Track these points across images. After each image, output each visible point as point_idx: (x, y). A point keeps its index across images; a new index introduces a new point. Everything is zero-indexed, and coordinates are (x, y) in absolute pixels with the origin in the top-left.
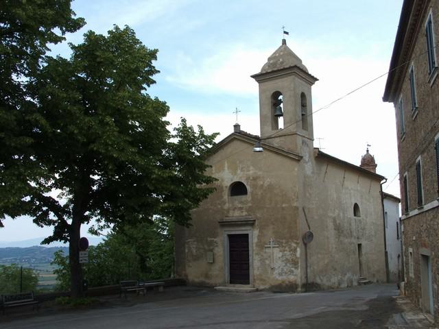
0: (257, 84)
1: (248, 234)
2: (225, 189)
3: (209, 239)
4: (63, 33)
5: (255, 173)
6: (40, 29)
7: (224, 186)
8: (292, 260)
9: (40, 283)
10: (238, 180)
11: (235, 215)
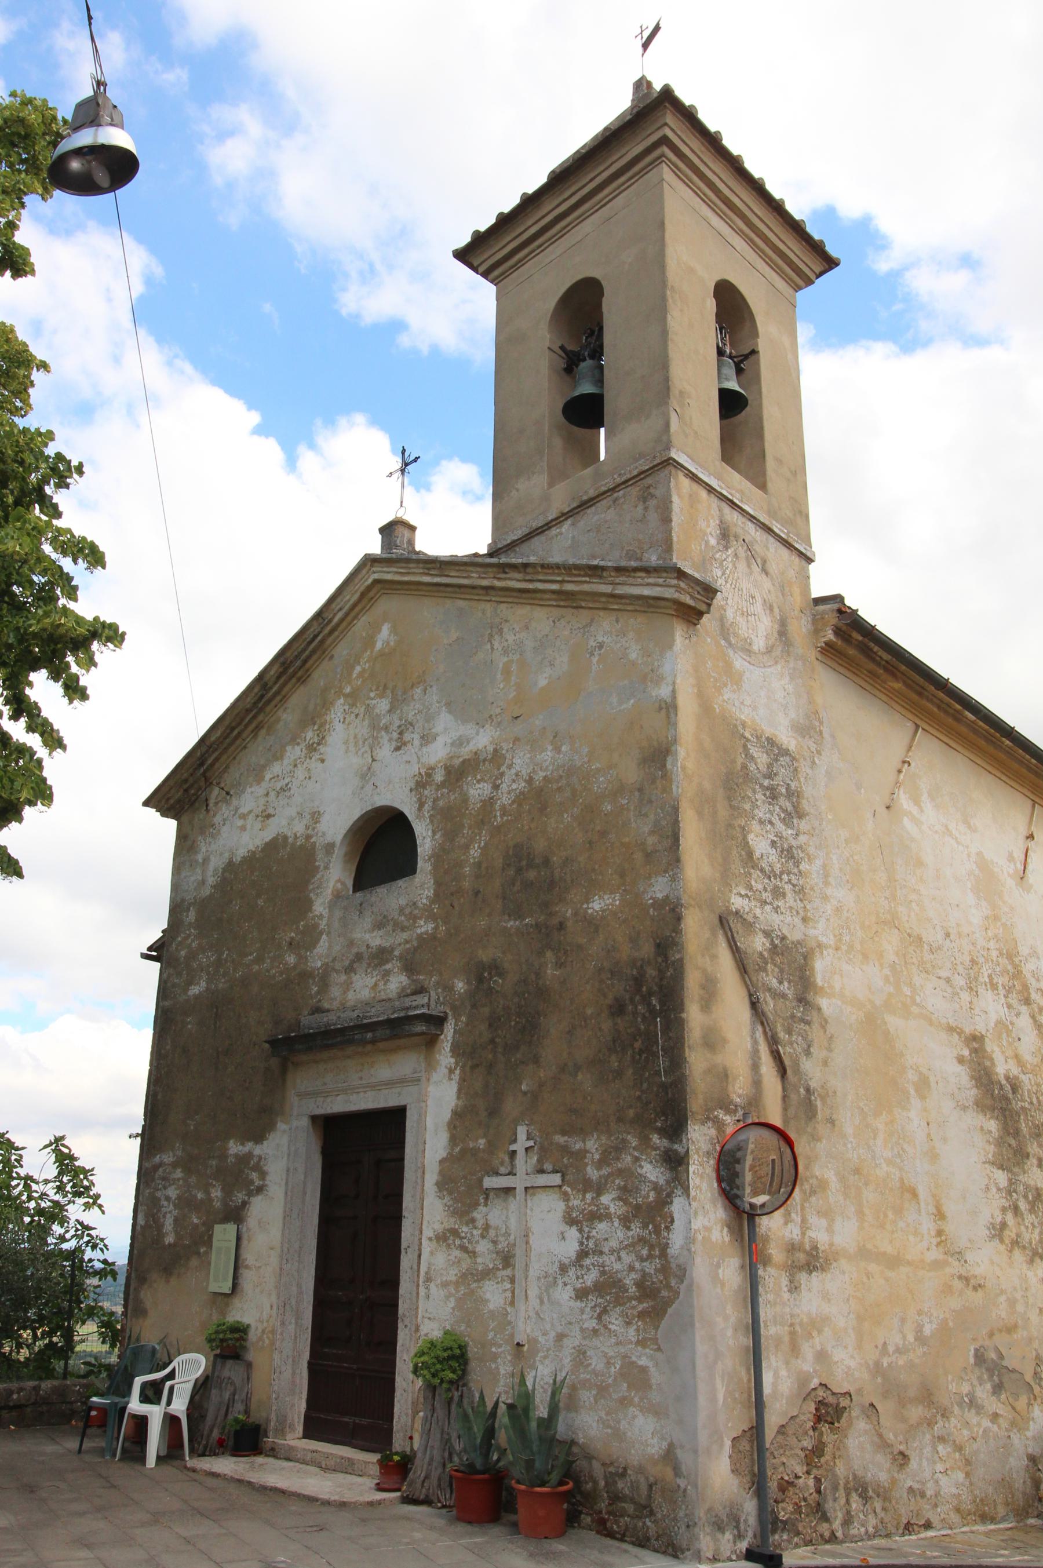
3: (234, 1148)
5: (460, 742)
7: (319, 841)
9: (1028, 1491)
10: (356, 814)
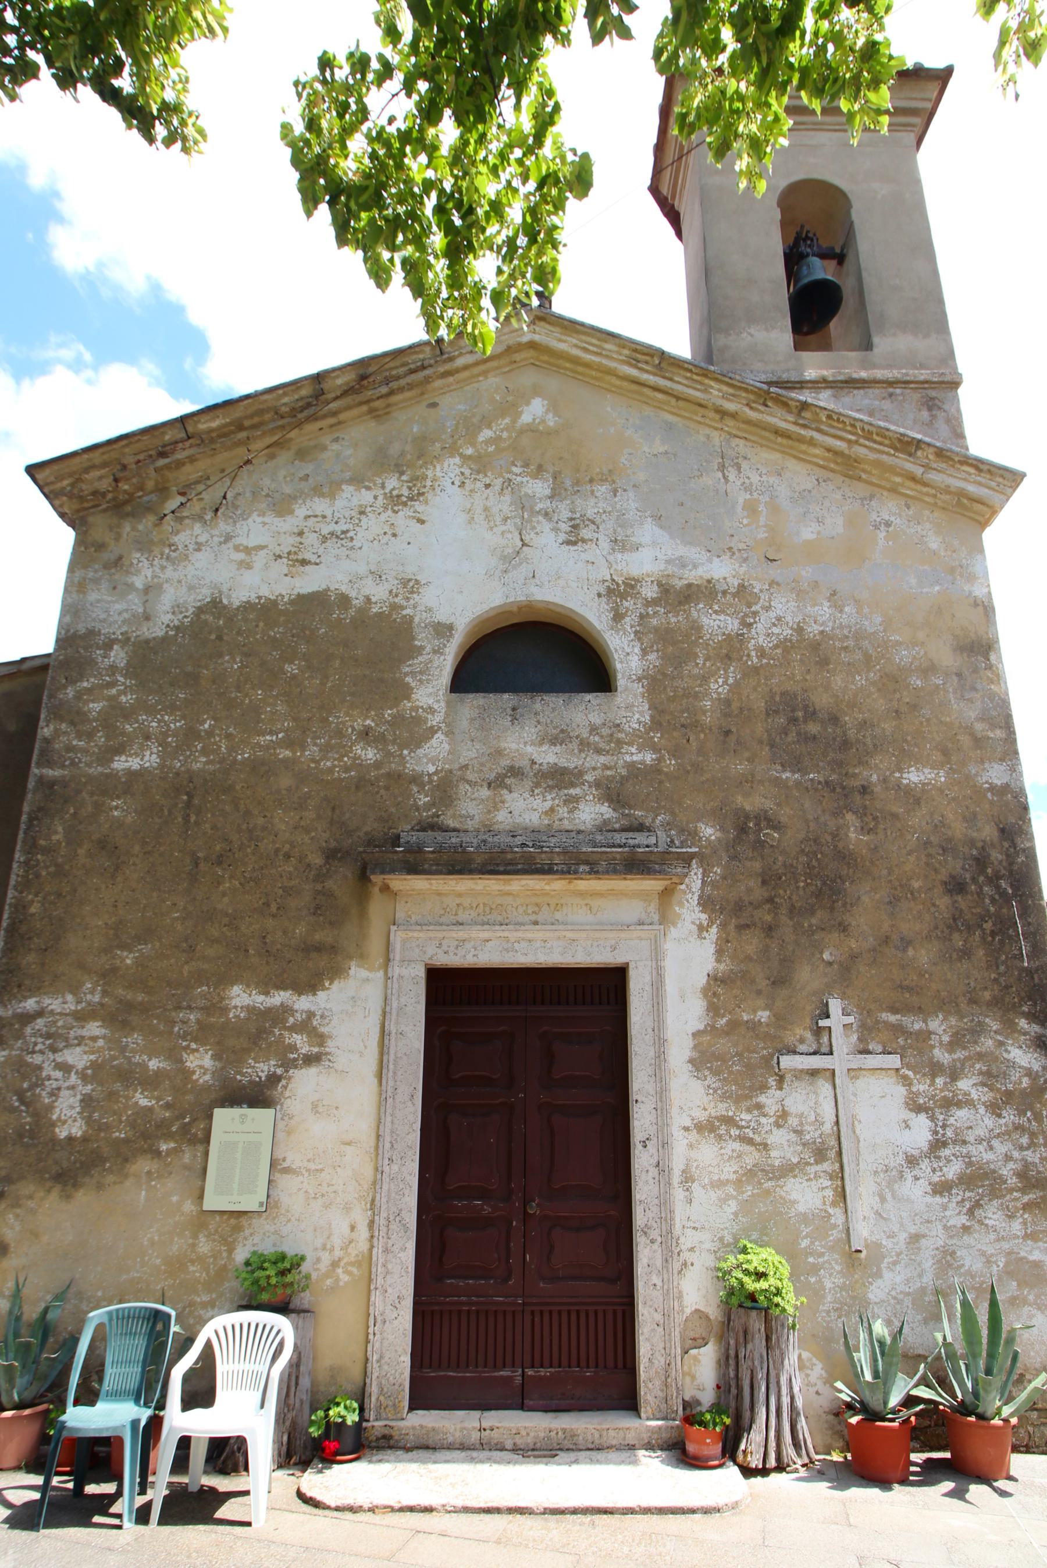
2: (423, 639)
8: (1022, 1175)
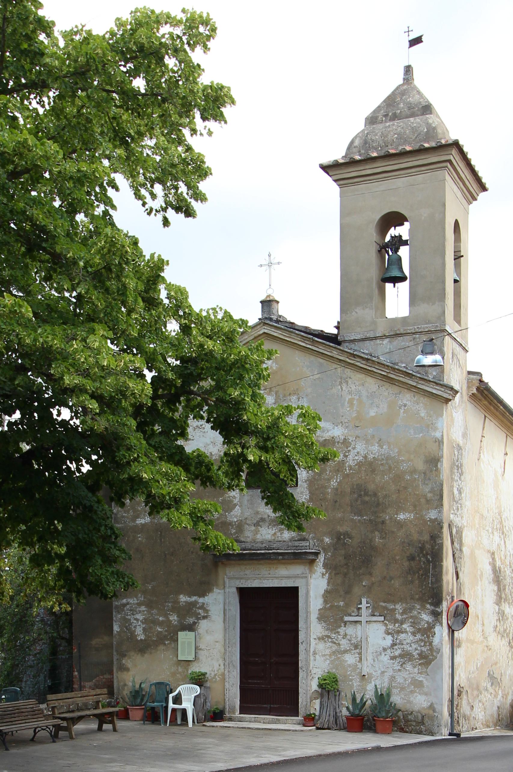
0: (334, 189)
1: (297, 588)
3: (183, 598)
4: (395, 606)
6: (18, 412)
11: (259, 537)
